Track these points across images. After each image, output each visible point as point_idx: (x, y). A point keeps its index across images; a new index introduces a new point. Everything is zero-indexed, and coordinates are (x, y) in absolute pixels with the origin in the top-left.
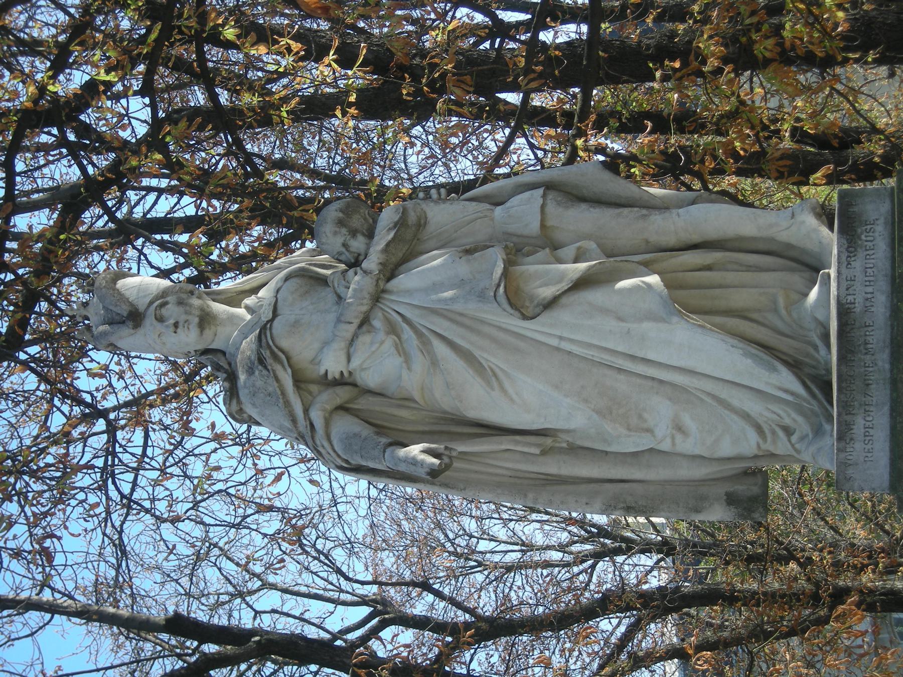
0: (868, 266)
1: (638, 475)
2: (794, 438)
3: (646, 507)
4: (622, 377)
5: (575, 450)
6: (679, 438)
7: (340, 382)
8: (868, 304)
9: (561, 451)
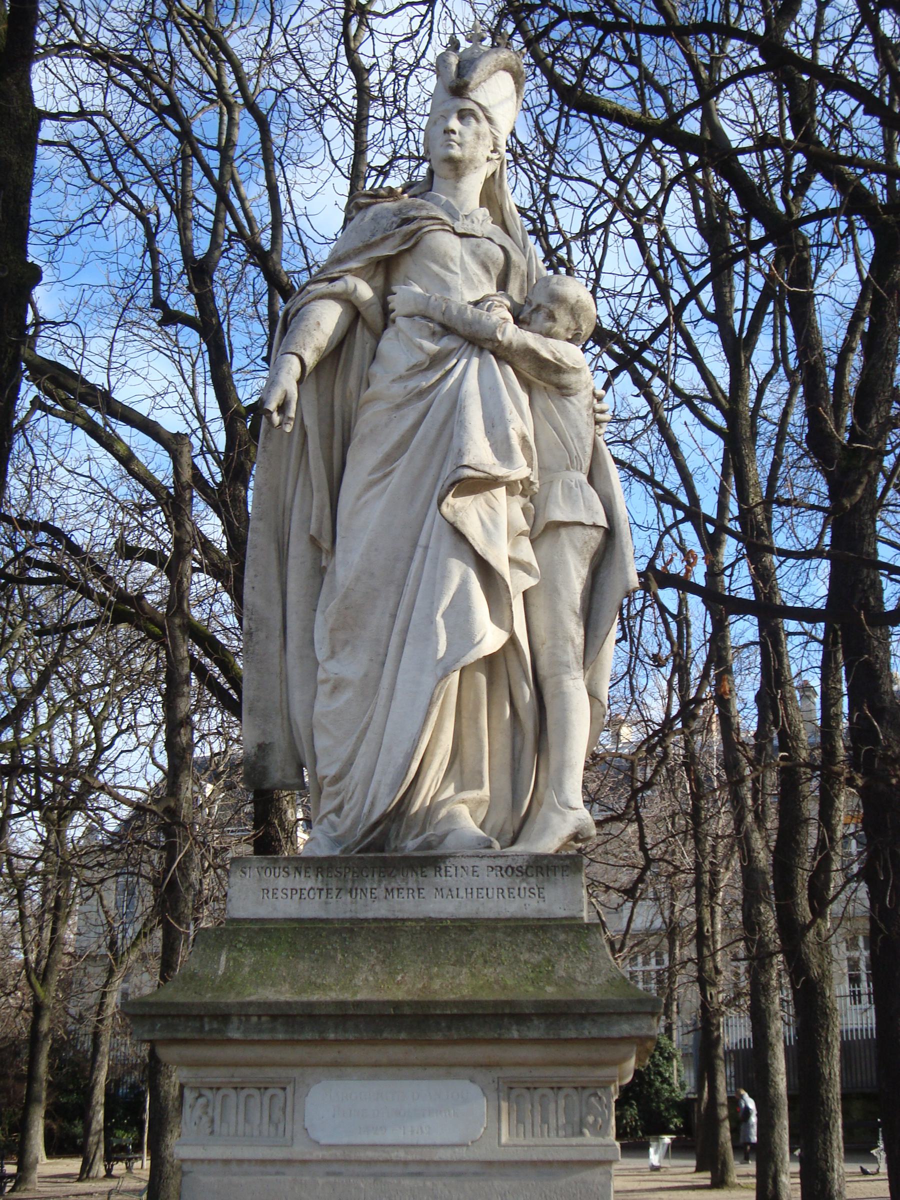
0: (490, 891)
1: (292, 646)
2: (332, 817)
3: (253, 653)
4: (387, 619)
5: (319, 573)
6: (327, 688)
7: (386, 312)
8: (445, 892)
9: (317, 560)
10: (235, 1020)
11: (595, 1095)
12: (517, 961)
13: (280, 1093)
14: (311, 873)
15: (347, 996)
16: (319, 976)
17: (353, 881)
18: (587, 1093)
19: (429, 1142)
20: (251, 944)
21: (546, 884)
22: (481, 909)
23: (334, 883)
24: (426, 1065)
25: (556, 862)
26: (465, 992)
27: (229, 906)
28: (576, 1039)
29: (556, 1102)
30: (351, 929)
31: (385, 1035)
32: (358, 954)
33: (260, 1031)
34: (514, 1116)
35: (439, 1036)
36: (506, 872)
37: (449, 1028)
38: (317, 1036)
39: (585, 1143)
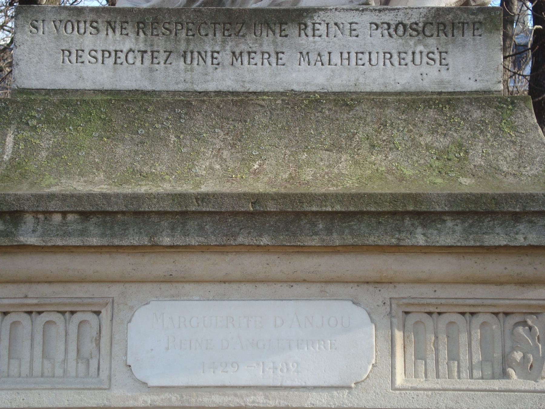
0: (374, 57)
8: (313, 57)
10: (29, 219)
11: (524, 323)
12: (417, 146)
13: (92, 318)
14: (130, 29)
15: (186, 188)
16: (146, 163)
17: (188, 41)
18: (511, 321)
19: (296, 383)
20: (48, 121)
21: (450, 47)
22: (362, 80)
23: (161, 44)
24: (292, 281)
25: (464, 17)
26: (349, 183)
27: (16, 72)
28: (506, 246)
29: (470, 335)
30: (186, 103)
31: (240, 239)
32: (197, 136)
33: (66, 234)
34: (411, 350)
35: (315, 241)
36: (396, 30)
37: (329, 231)
38: (146, 241)
39: (511, 387)
